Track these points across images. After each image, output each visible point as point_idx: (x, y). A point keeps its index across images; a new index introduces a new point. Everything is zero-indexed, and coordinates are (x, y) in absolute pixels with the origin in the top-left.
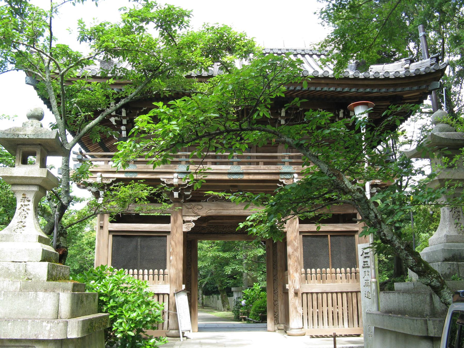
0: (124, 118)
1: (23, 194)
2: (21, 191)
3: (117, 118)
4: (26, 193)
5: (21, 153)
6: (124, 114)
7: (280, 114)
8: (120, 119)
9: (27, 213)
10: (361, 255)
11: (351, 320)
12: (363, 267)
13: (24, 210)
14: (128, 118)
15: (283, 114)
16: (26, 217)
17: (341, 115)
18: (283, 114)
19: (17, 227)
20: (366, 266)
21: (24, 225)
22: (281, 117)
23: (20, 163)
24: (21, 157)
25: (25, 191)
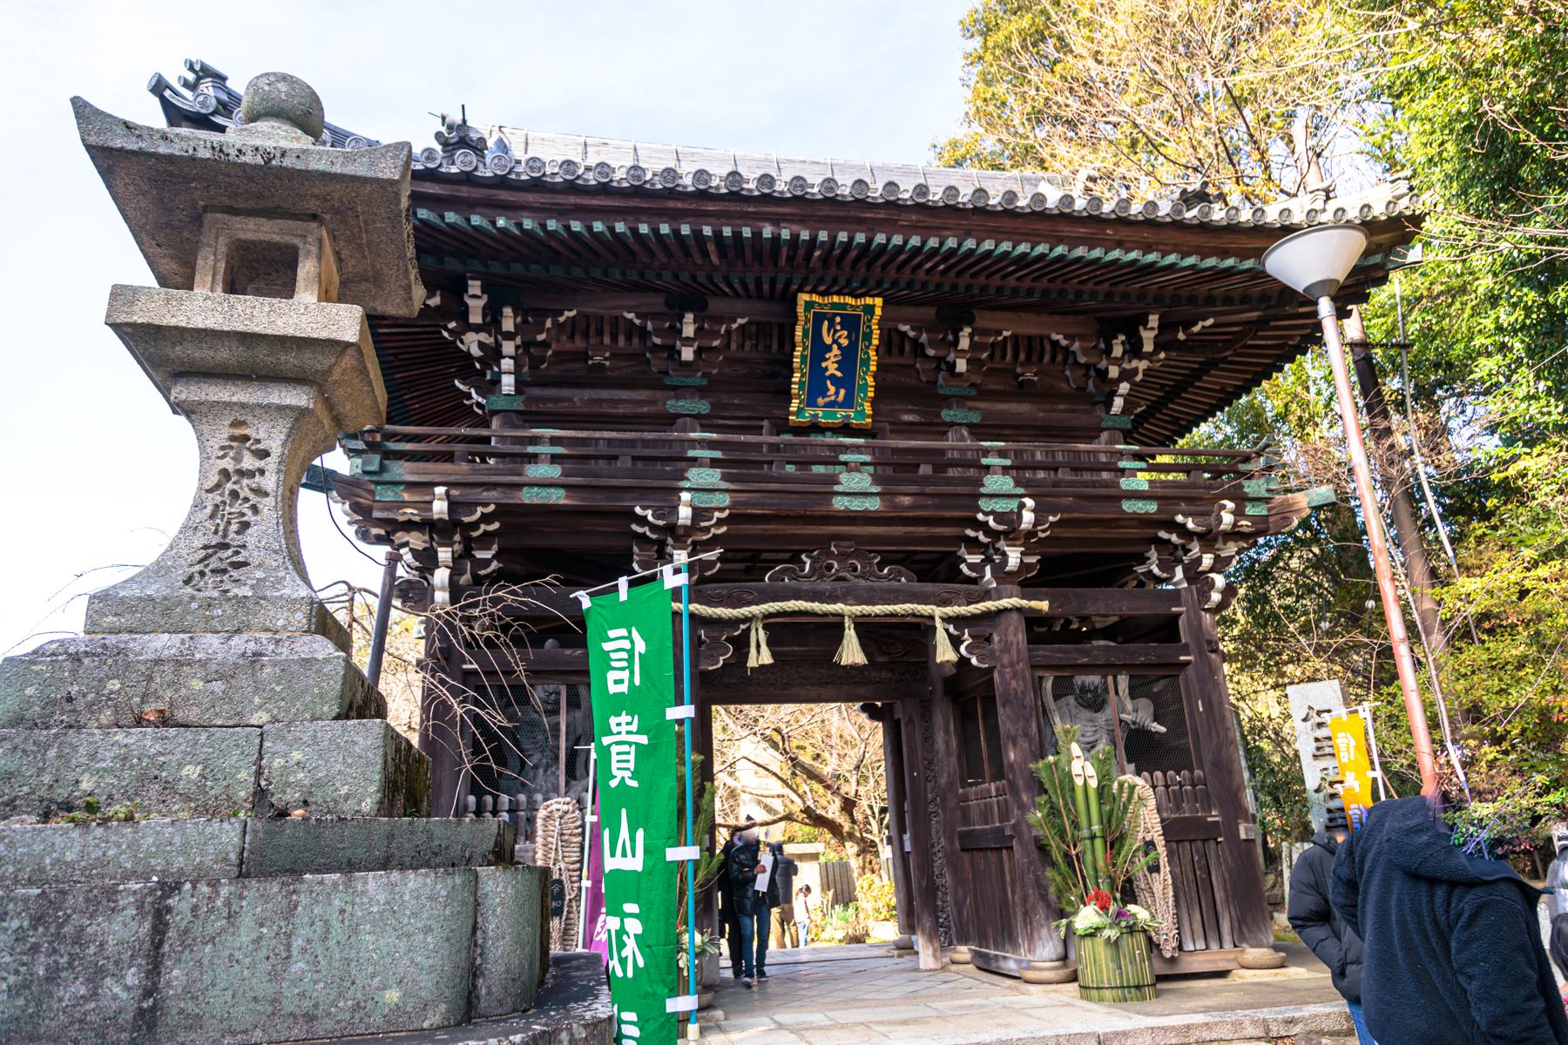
0: (509, 336)
1: (236, 424)
2: (227, 405)
3: (483, 337)
4: (249, 418)
5: (223, 249)
6: (508, 324)
7: (956, 342)
8: (492, 340)
9: (255, 509)
10: (1305, 720)
11: (1210, 923)
12: (1315, 757)
13: (235, 495)
14: (518, 340)
15: (964, 343)
16: (245, 526)
17: (1118, 351)
18: (964, 343)
19: (197, 568)
20: (1327, 750)
21: (240, 558)
22: (956, 350)
23: (219, 288)
24: (222, 266)
25: (243, 406)
